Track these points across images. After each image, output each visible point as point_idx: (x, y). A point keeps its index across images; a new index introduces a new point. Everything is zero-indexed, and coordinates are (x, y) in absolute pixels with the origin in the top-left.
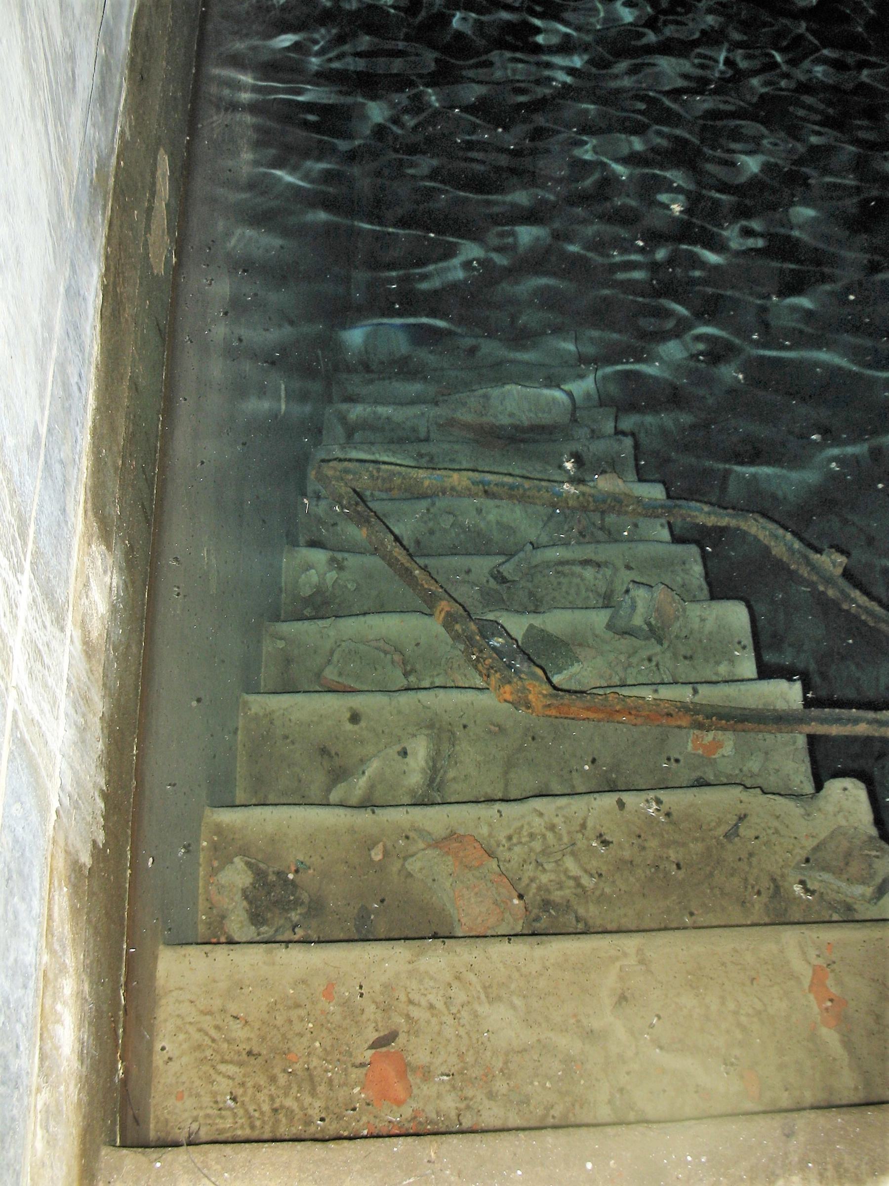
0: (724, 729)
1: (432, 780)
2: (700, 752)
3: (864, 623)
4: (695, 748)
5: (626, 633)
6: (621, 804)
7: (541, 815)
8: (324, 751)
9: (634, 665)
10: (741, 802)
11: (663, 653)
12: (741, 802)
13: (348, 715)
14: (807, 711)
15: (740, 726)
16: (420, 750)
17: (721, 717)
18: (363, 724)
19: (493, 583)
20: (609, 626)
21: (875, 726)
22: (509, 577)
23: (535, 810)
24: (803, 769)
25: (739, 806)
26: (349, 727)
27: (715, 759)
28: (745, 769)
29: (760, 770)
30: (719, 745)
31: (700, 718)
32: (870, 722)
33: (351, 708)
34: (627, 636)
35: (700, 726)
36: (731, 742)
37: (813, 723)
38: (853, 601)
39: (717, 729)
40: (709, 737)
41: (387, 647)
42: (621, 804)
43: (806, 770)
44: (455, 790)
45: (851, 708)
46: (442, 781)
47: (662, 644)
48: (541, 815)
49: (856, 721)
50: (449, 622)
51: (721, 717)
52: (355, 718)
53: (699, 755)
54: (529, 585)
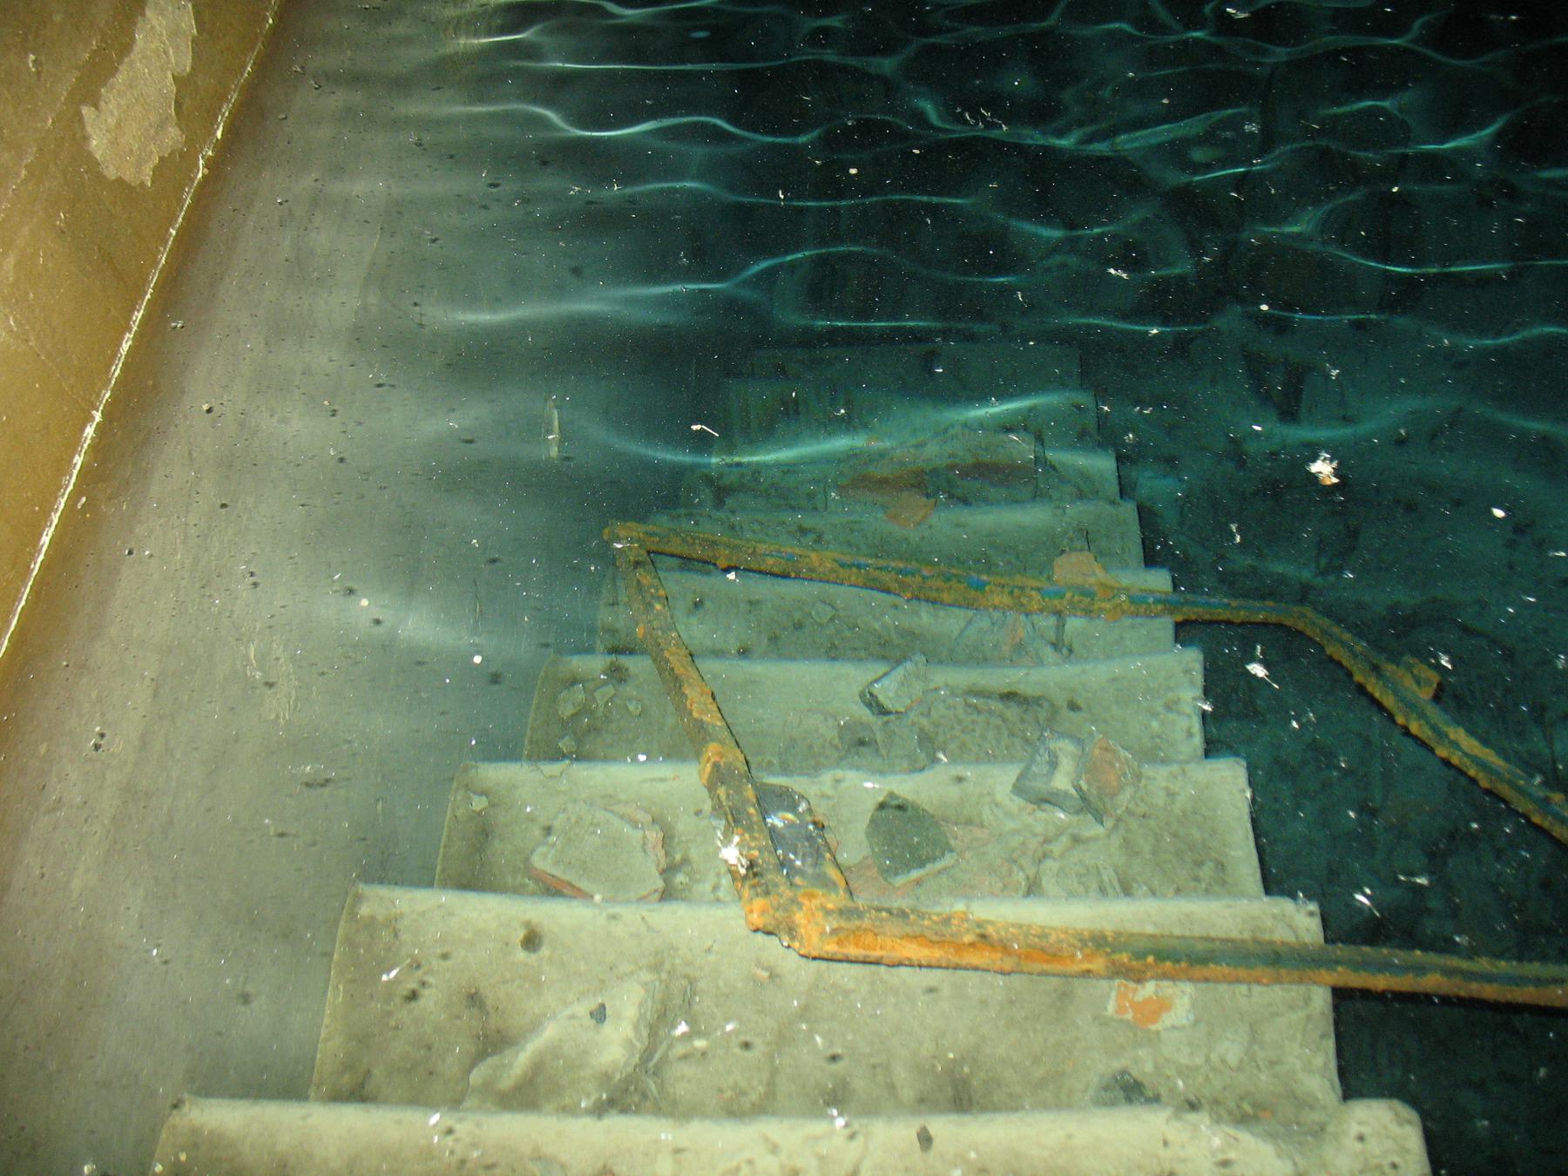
0: (1172, 977)
1: (647, 1055)
2: (1129, 1016)
3: (1473, 781)
4: (1121, 1009)
5: (1047, 801)
6: (925, 1140)
7: (774, 1149)
8: (474, 999)
9: (1056, 854)
10: (1165, 1143)
11: (1108, 836)
12: (1165, 1143)
13: (521, 934)
14: (1330, 947)
15: (1198, 971)
16: (629, 1004)
17: (1161, 956)
18: (545, 951)
19: (865, 714)
20: (1018, 789)
21: (1457, 980)
22: (888, 705)
23: (766, 1139)
24: (1319, 1061)
25: (1162, 1152)
26: (521, 955)
27: (1158, 1032)
28: (1213, 1056)
29: (1241, 1061)
30: (1162, 1006)
31: (1124, 957)
32: (1449, 972)
33: (527, 924)
34: (1046, 806)
35: (1116, 971)
36: (1186, 999)
37: (1340, 969)
38: (1455, 745)
39: (1158, 977)
40: (1149, 989)
41: (640, 816)
42: (925, 1140)
43: (1325, 1064)
44: (684, 1080)
45: (1412, 948)
46: (664, 1059)
47: (1102, 823)
48: (774, 1149)
49: (1421, 970)
50: (719, 776)
51: (1161, 956)
52: (532, 941)
53: (1127, 1022)
54: (924, 722)
